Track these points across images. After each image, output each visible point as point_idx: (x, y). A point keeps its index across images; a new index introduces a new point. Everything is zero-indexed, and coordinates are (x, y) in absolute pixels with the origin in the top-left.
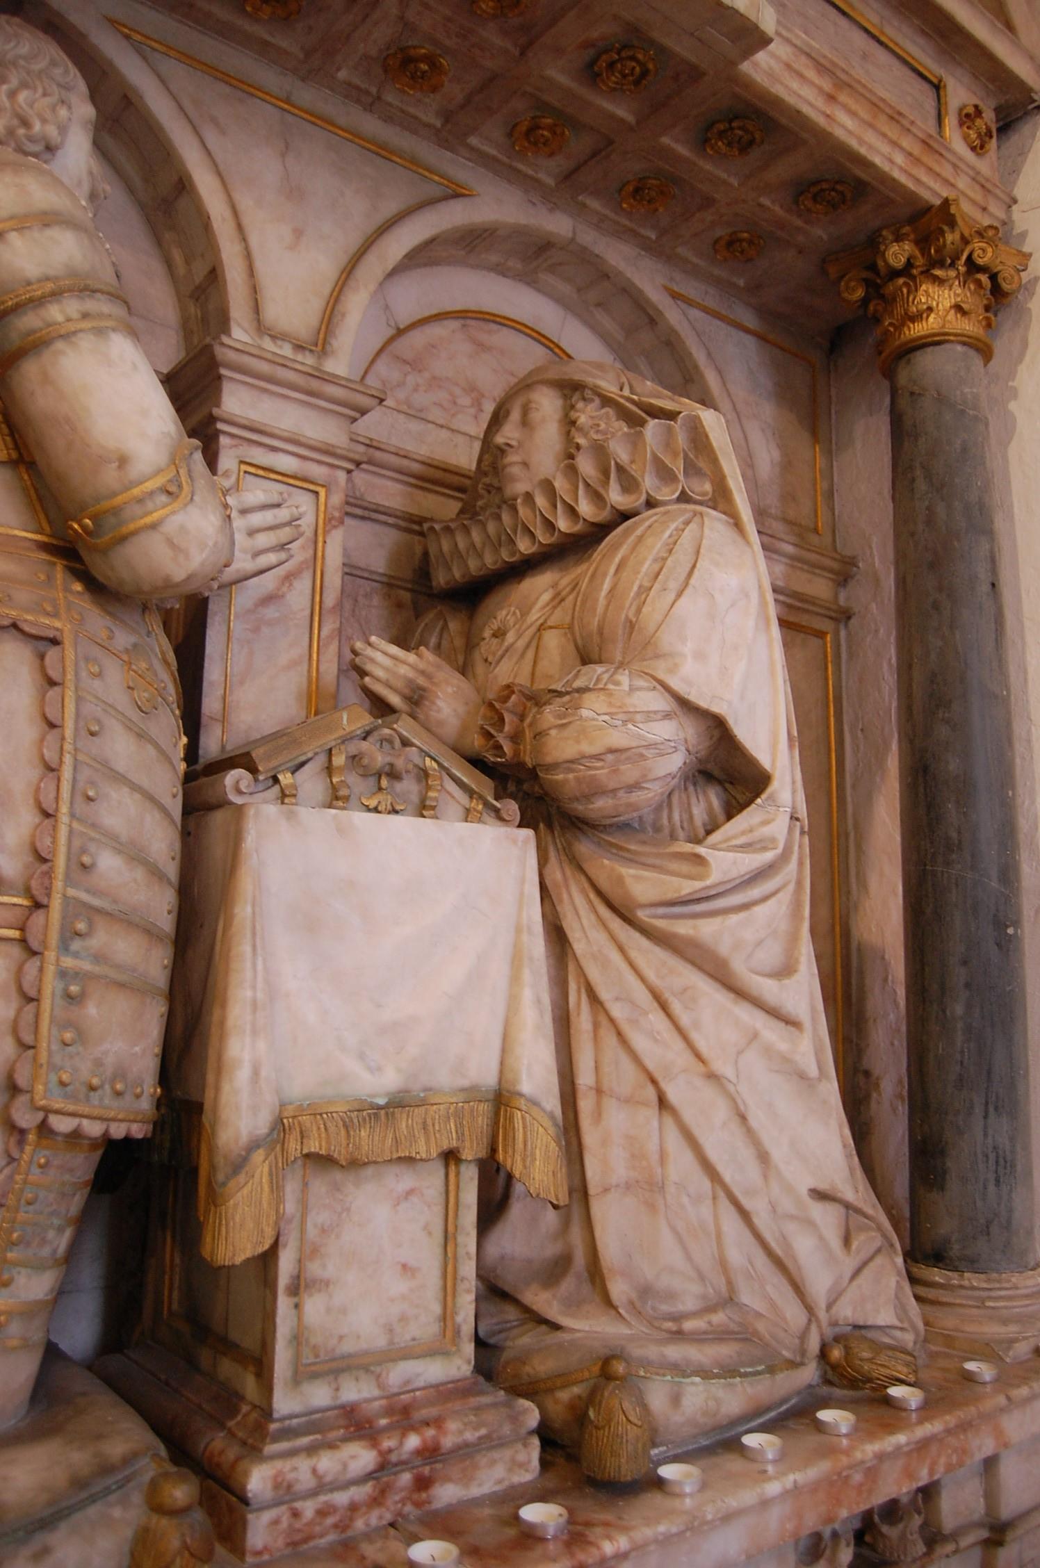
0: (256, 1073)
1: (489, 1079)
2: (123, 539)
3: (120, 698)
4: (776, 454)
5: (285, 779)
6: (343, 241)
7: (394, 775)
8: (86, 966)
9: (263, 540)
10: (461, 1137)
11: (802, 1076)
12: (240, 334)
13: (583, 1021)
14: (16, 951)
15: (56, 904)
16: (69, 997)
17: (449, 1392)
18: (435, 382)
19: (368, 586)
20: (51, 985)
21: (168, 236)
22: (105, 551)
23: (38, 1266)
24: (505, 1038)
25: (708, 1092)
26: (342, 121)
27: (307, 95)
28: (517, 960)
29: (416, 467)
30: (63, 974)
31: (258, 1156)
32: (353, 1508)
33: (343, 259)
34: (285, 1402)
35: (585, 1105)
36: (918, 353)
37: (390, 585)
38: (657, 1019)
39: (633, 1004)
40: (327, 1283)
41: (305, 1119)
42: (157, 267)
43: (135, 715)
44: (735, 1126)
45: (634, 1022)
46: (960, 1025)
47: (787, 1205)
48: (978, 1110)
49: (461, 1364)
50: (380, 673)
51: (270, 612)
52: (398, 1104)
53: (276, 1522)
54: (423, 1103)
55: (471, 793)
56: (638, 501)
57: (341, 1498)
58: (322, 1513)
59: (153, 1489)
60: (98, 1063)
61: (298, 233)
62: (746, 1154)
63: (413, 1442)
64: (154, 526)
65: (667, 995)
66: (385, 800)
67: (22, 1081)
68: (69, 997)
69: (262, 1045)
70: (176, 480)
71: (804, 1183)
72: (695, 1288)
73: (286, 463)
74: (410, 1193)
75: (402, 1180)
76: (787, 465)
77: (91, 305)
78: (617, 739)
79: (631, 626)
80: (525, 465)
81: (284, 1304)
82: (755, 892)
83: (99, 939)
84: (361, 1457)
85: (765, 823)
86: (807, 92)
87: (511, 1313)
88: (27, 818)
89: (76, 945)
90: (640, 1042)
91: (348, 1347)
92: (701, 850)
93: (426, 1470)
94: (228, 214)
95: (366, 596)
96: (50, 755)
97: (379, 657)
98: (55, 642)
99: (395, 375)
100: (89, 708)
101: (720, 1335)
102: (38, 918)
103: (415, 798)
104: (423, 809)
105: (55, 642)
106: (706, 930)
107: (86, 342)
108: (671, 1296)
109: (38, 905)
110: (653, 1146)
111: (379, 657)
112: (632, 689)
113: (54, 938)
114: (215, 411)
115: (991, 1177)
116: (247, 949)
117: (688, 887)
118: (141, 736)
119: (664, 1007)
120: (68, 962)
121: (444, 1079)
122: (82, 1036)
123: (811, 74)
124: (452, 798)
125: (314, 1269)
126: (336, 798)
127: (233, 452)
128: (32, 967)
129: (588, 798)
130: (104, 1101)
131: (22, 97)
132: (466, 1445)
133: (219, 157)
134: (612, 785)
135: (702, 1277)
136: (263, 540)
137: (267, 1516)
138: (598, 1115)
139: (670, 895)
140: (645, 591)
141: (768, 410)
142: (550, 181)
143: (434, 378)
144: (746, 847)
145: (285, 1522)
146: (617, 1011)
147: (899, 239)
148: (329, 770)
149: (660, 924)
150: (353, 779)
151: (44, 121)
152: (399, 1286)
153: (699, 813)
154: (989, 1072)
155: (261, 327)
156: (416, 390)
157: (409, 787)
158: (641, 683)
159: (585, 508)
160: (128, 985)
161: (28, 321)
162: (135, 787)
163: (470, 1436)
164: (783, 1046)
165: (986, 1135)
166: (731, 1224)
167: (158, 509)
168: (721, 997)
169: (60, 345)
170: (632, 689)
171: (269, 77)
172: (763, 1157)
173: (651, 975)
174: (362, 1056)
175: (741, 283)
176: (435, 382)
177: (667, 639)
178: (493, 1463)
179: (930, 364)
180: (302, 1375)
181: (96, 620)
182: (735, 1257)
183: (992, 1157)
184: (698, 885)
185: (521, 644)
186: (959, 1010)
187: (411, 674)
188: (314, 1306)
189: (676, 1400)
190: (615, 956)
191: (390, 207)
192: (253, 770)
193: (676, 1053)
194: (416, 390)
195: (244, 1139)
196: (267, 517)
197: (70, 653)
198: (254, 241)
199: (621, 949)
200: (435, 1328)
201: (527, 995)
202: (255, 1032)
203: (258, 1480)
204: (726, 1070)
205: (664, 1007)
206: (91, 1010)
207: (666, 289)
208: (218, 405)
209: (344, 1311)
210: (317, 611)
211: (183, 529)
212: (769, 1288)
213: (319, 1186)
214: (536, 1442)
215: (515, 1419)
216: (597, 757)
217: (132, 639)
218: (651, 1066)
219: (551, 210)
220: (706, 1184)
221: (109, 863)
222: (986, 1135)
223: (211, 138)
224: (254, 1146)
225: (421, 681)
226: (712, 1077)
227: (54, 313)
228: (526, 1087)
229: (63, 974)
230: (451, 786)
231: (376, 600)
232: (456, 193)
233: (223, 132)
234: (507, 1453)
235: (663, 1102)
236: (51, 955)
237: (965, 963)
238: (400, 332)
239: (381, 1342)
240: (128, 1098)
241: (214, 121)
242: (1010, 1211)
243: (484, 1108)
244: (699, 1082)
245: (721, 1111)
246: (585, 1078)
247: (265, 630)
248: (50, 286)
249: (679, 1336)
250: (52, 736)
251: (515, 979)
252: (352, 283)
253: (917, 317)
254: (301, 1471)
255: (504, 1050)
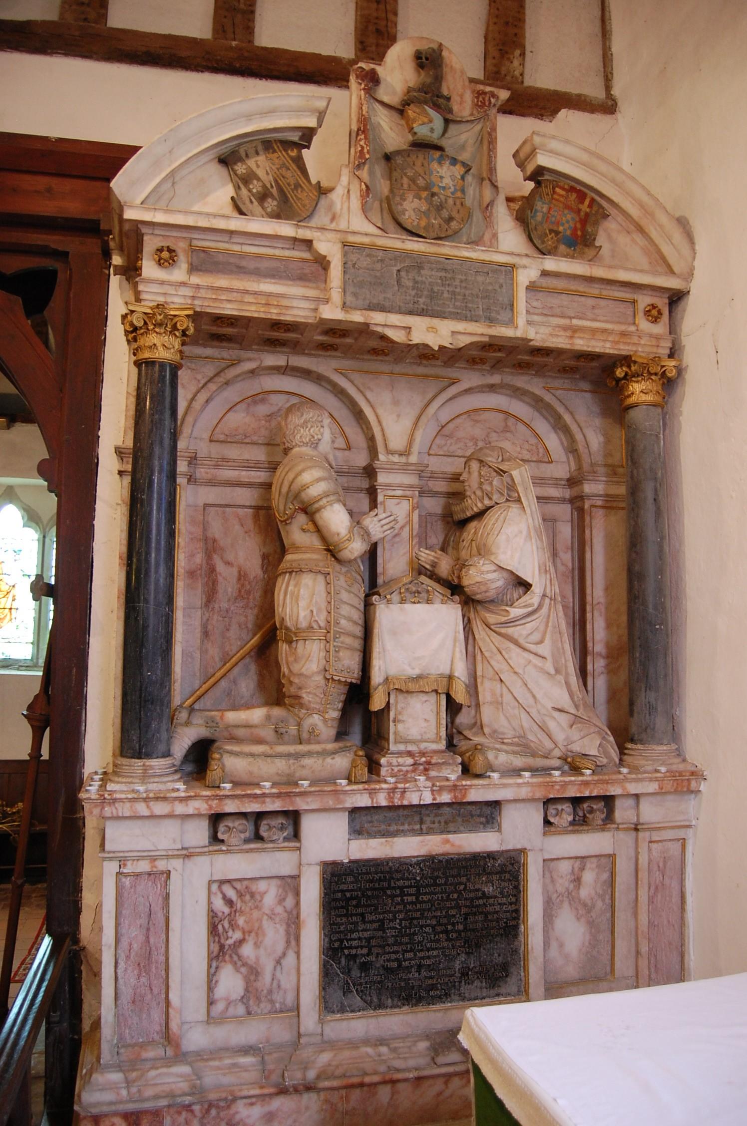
0: (380, 668)
1: (447, 672)
2: (340, 551)
3: (344, 585)
4: (601, 439)
5: (388, 597)
6: (412, 414)
7: (419, 593)
8: (340, 644)
9: (386, 527)
10: (438, 686)
11: (548, 674)
12: (382, 457)
13: (479, 657)
14: (325, 642)
15: (332, 631)
16: (336, 651)
17: (436, 752)
18: (459, 440)
19: (436, 518)
20: (332, 649)
21: (361, 421)
22: (337, 553)
23: (334, 710)
24: (452, 661)
25: (515, 677)
26: (411, 372)
27: (398, 368)
28: (455, 640)
29: (449, 476)
30: (334, 646)
31: (380, 687)
32: (407, 771)
33: (414, 419)
34: (393, 747)
35: (479, 680)
36: (631, 410)
37: (444, 517)
38: (499, 657)
39: (492, 652)
40: (404, 721)
41: (395, 680)
42: (359, 430)
43: (348, 587)
44: (524, 687)
45: (491, 657)
46: (638, 660)
47: (543, 711)
48: (643, 690)
49: (442, 745)
50: (423, 559)
51: (397, 539)
52: (419, 677)
53: (388, 770)
54: (427, 678)
55: (443, 595)
56: (492, 503)
57: (404, 769)
58: (399, 771)
59: (356, 752)
60: (343, 665)
61: (398, 416)
62: (529, 696)
63: (423, 759)
64: (346, 548)
65: (501, 650)
66: (416, 600)
67: (327, 669)
68: (336, 651)
69: (381, 662)
70: (350, 537)
71: (549, 705)
72: (512, 732)
73: (399, 493)
74: (426, 701)
75: (424, 697)
76: (608, 441)
77: (328, 499)
78: (478, 579)
79: (485, 545)
80: (469, 486)
81: (391, 724)
82: (529, 619)
83: (342, 639)
84: (410, 761)
85: (531, 599)
86: (560, 340)
87: (462, 737)
88: (325, 613)
89: (337, 640)
90: (493, 663)
91: (410, 737)
92: (507, 608)
93: (427, 767)
94: (375, 418)
95: (436, 521)
96: (329, 600)
97: (423, 554)
98: (329, 574)
99: (443, 442)
100: (337, 588)
101: (518, 745)
102: (329, 634)
103: (426, 598)
104: (429, 601)
105: (329, 574)
106: (510, 631)
107: (328, 508)
108: (503, 733)
109: (328, 632)
110: (498, 691)
111: (423, 554)
112: (483, 564)
113: (332, 639)
114: (375, 484)
115: (648, 712)
116: (377, 640)
117: (503, 619)
118: (350, 592)
119: (501, 653)
120: (335, 644)
121: (433, 671)
122: (339, 660)
123: (562, 333)
124: (438, 597)
125: (400, 717)
126: (403, 601)
127: (382, 494)
128: (328, 644)
129: (475, 595)
130: (345, 674)
131: (311, 431)
132: (439, 763)
133: (371, 400)
134: (479, 592)
135: (514, 729)
136: (386, 527)
137: (385, 769)
138: (482, 683)
139: (499, 622)
140: (488, 534)
141: (598, 422)
142: (488, 368)
143: (458, 439)
144: (525, 606)
145: (390, 771)
146: (487, 654)
147: (621, 366)
148: (400, 593)
149: (497, 629)
150: (407, 595)
151: (317, 435)
152: (424, 724)
153: (516, 596)
154: (647, 677)
155: (389, 452)
156: (451, 445)
157: (424, 595)
158: (487, 562)
159: (480, 505)
160: (350, 648)
161: (316, 506)
162: (348, 604)
163: (440, 761)
164: (540, 665)
165: (645, 698)
166: (524, 715)
167: (346, 544)
168: (518, 650)
169: (323, 510)
170: (483, 564)
171: (385, 368)
172: (534, 696)
173: (497, 644)
174: (409, 665)
175: (578, 376)
176: (459, 440)
177: (494, 550)
178: (447, 769)
179: (633, 414)
180: (396, 742)
181: (338, 567)
182: (525, 725)
183: (648, 705)
184: (506, 618)
185: (467, 545)
186: (638, 655)
187: (433, 559)
188: (400, 726)
189: (496, 757)
190: (487, 639)
191: (429, 396)
192: (380, 595)
193: (505, 666)
194: (451, 445)
195: (377, 683)
196: (387, 520)
197: (332, 577)
198: (384, 424)
199: (489, 637)
200: (435, 736)
201: (457, 650)
202: (379, 659)
203: (383, 761)
204: (520, 671)
205: (501, 653)
206: (341, 654)
207: (544, 387)
208: (376, 481)
209: (408, 729)
210: (412, 537)
211: (352, 548)
212: (539, 736)
213: (401, 697)
214: (460, 766)
215: (453, 759)
216: (474, 584)
217: (346, 569)
218: (496, 669)
219: (491, 375)
220: (517, 704)
221: (343, 622)
222: (645, 698)
223: (369, 395)
224: (379, 685)
225: (436, 560)
226: (515, 673)
227: (321, 503)
228: (456, 674)
229: (334, 646)
230: (436, 593)
231: (439, 523)
232: (453, 382)
233: (372, 391)
234: (451, 767)
235: (501, 680)
236: (331, 642)
237: (639, 638)
238: (443, 427)
239: (419, 737)
240: (351, 673)
241: (369, 388)
242: (655, 724)
243: (446, 680)
244: (512, 674)
245: (520, 683)
246: (479, 673)
247: (395, 545)
248: (319, 497)
249: (503, 743)
250: (329, 595)
251: (454, 646)
252: (417, 428)
253: (629, 396)
254: (394, 761)
255: (452, 665)
